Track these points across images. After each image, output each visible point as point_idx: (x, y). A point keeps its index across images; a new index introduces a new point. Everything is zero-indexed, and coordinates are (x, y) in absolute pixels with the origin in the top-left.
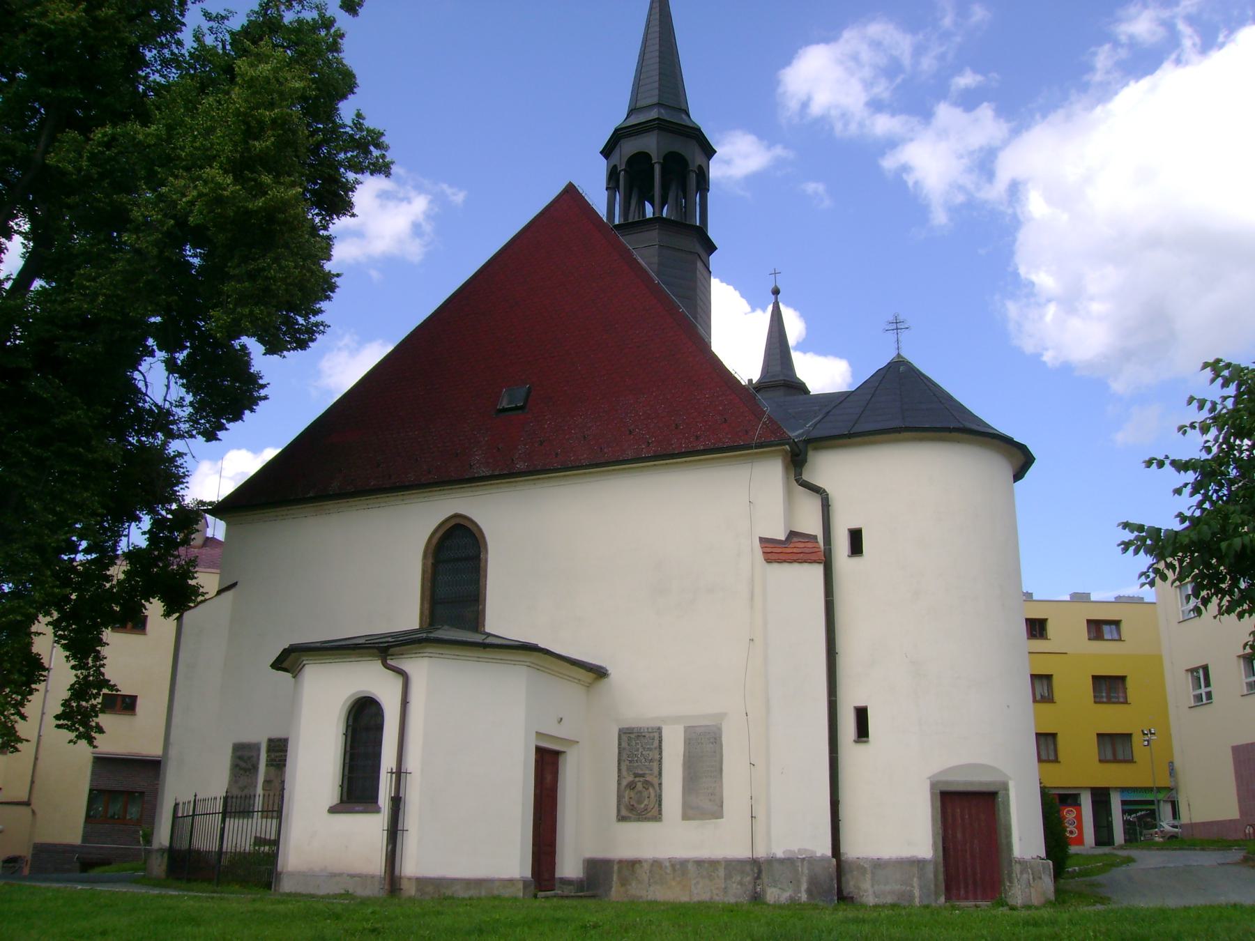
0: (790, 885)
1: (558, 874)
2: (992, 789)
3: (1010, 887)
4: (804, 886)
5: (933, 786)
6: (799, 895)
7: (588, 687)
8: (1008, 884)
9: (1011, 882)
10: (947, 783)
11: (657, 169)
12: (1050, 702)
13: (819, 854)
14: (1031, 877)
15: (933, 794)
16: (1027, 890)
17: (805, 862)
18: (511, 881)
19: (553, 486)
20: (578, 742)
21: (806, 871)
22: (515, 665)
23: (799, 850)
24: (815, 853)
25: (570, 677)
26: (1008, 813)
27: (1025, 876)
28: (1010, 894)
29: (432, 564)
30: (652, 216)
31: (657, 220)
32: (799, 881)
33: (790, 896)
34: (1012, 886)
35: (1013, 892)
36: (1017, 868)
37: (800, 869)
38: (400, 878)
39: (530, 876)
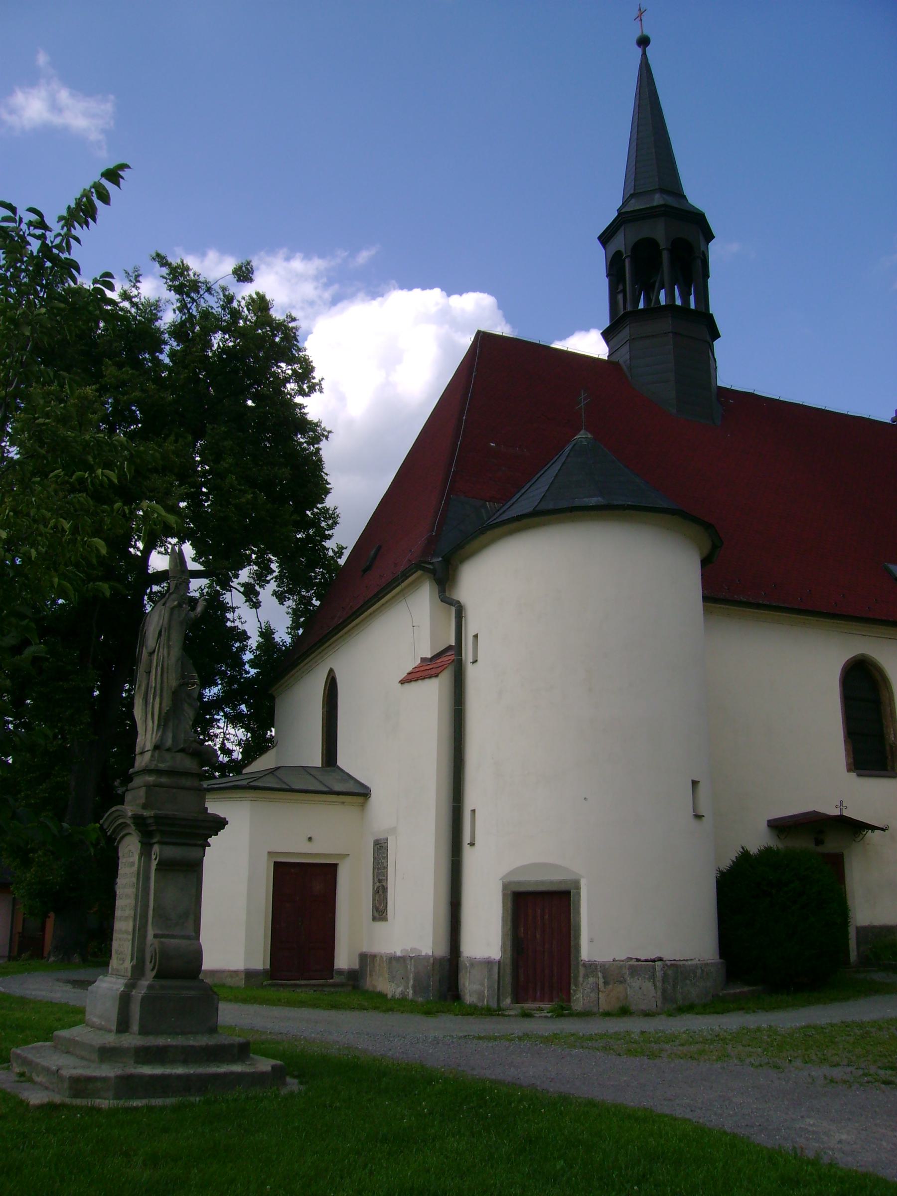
0: (402, 981)
1: (336, 967)
2: (563, 888)
3: (575, 991)
4: (411, 983)
5: (505, 886)
6: (408, 990)
7: (363, 806)
8: (574, 988)
9: (576, 985)
10: (519, 883)
11: (665, 256)
12: (694, 781)
13: (423, 954)
14: (601, 981)
15: (504, 895)
16: (592, 995)
17: (413, 960)
18: (236, 972)
19: (357, 634)
20: (349, 855)
21: (413, 969)
22: (241, 801)
23: (411, 949)
24: (421, 952)
25: (314, 801)
26: (578, 913)
27: (591, 980)
28: (575, 998)
29: (327, 711)
30: (664, 304)
31: (671, 307)
32: (408, 978)
33: (402, 990)
34: (577, 990)
35: (577, 996)
36: (582, 971)
37: (409, 967)
38: (264, 969)
39: (269, 967)
